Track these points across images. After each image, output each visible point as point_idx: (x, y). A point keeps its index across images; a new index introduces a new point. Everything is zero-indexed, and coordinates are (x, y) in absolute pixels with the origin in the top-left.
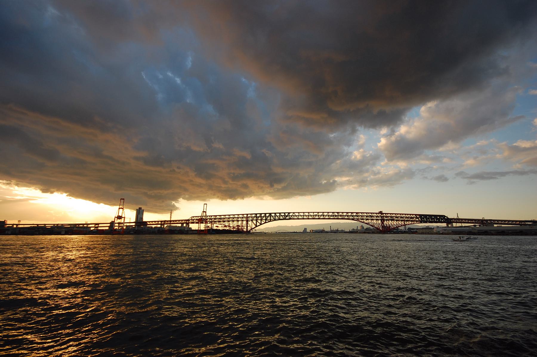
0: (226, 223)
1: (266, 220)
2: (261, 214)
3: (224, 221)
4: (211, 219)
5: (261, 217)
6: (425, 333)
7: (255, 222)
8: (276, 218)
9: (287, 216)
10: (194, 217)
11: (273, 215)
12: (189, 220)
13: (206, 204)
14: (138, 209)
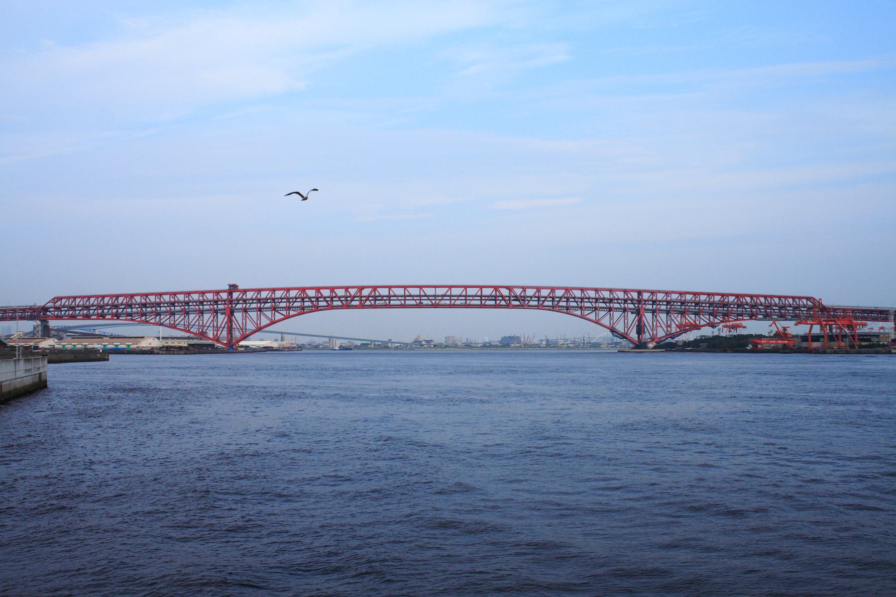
0: (162, 317)
4: (117, 307)
9: (353, 298)
10: (60, 299)
12: (45, 309)
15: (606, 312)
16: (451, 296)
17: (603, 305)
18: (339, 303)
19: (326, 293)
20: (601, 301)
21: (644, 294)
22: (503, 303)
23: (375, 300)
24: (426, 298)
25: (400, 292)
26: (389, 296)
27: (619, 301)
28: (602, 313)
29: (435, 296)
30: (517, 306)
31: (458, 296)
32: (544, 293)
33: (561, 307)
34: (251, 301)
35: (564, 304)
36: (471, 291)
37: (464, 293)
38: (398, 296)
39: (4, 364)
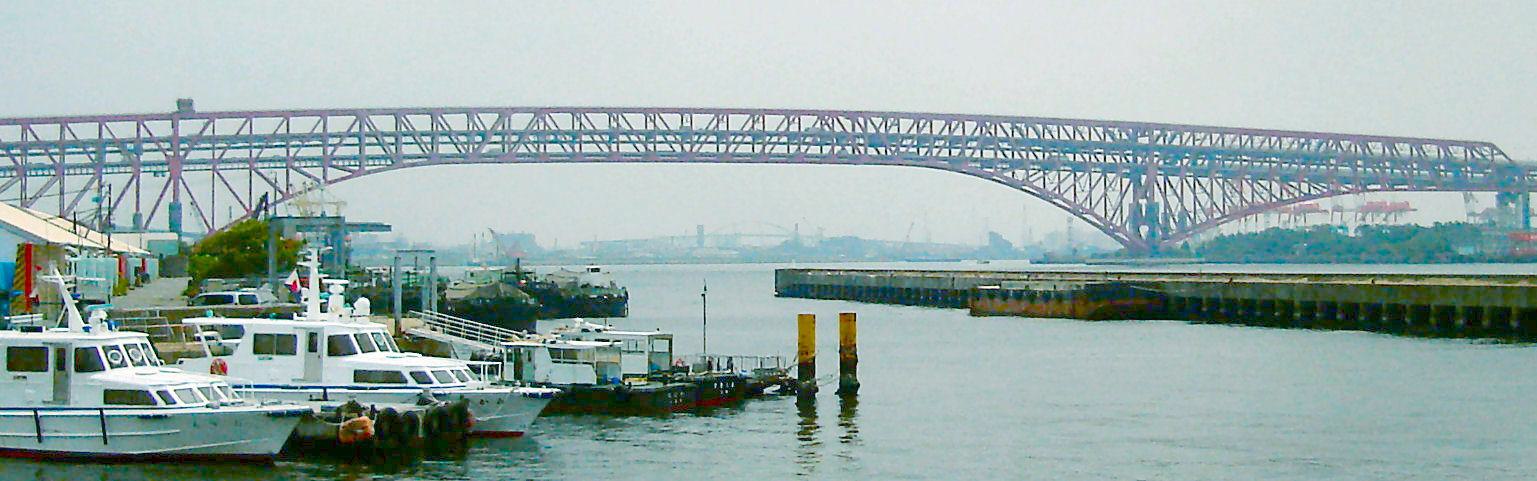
17: (46, 160)
19: (422, 123)
20: (552, 138)
21: (515, 117)
23: (24, 154)
24: (153, 146)
27: (670, 138)
30: (452, 156)
34: (739, 139)
39: (1536, 159)
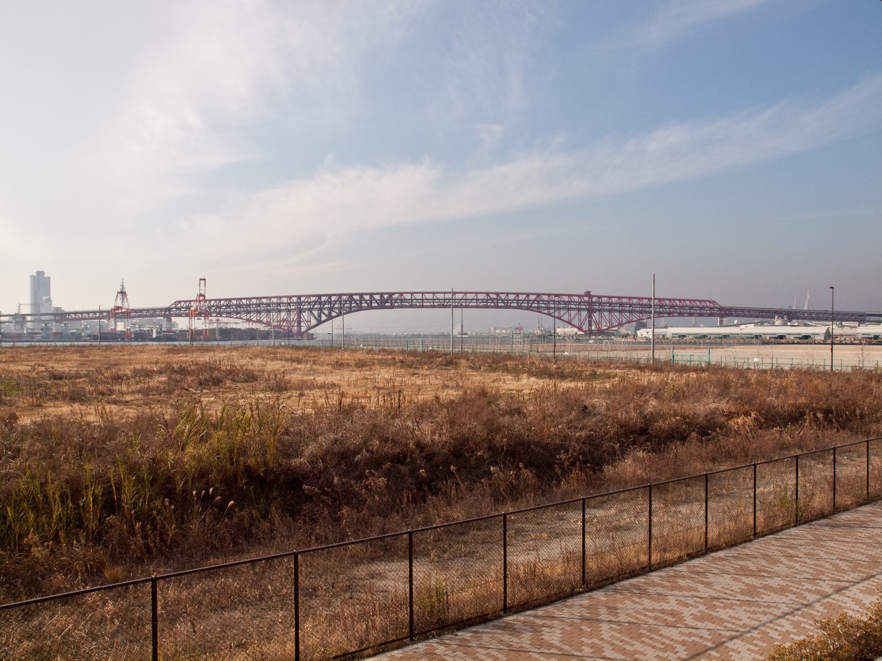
1: (331, 309)
2: (330, 296)
3: (248, 312)
4: (220, 307)
5: (340, 302)
6: (818, 588)
7: (316, 313)
8: (363, 305)
10: (180, 302)
11: (356, 297)
12: (169, 309)
13: (205, 280)
14: (35, 275)
15: (565, 311)
16: (466, 299)
18: (502, 304)
22: (492, 304)
23: (402, 302)
25: (430, 296)
26: (423, 299)
28: (562, 312)
29: (444, 299)
31: (471, 300)
32: (522, 297)
33: (534, 307)
35: (536, 305)
36: (469, 296)
37: (475, 298)
38: (428, 300)
